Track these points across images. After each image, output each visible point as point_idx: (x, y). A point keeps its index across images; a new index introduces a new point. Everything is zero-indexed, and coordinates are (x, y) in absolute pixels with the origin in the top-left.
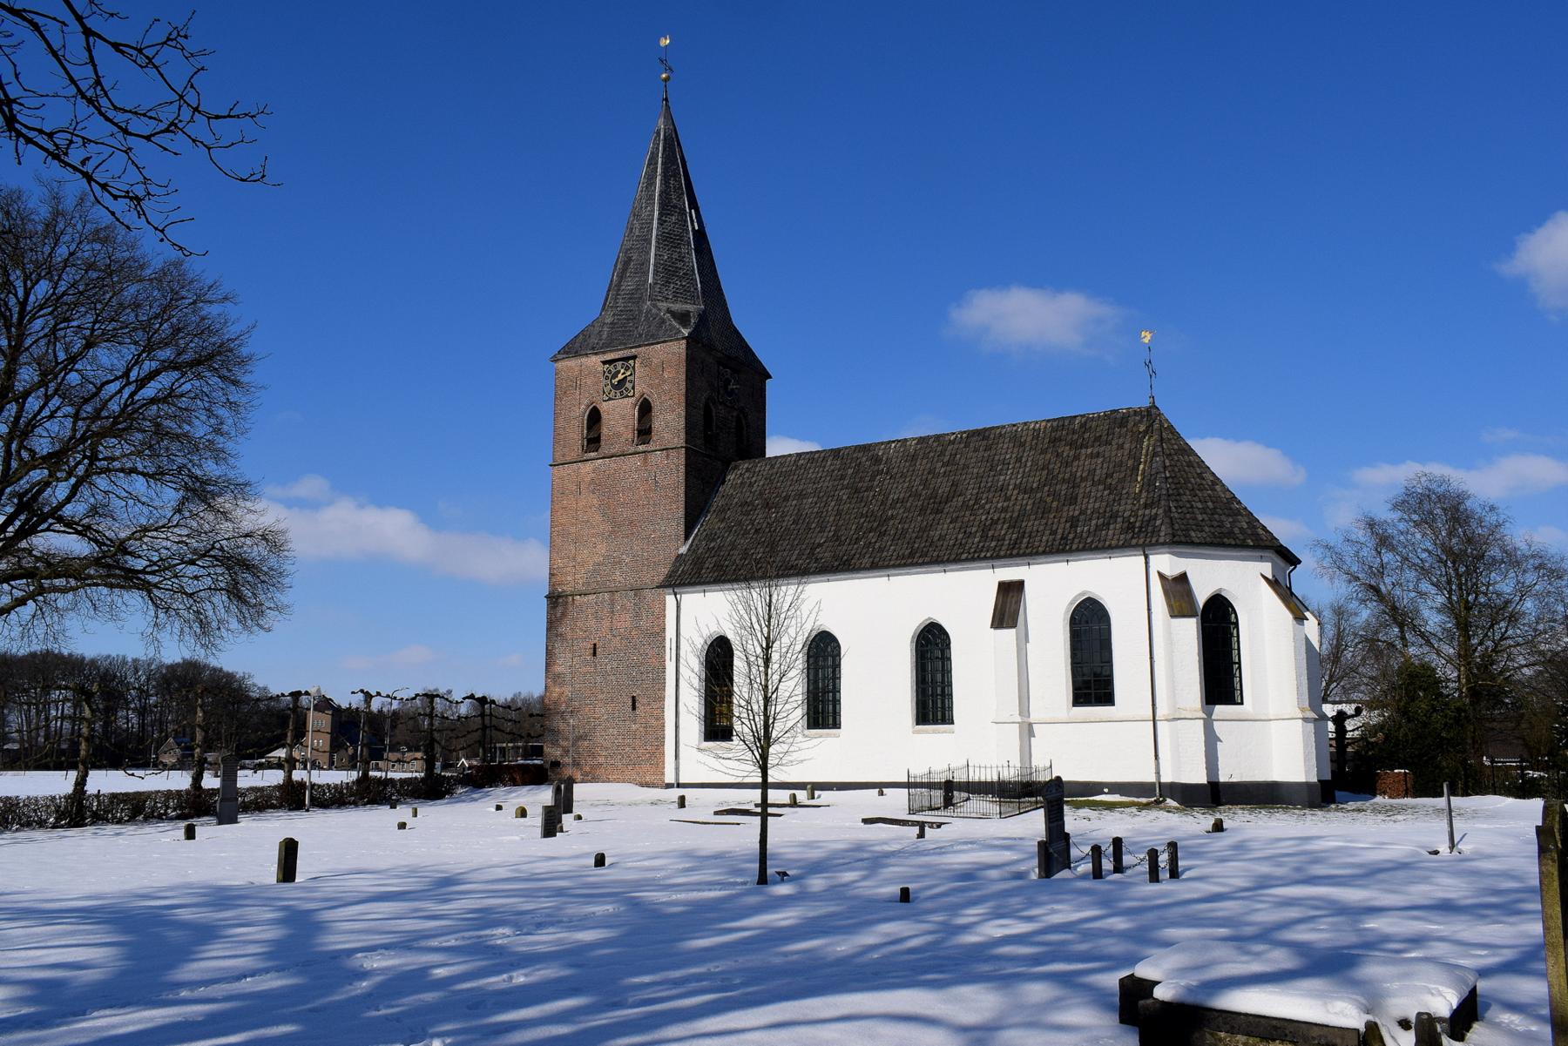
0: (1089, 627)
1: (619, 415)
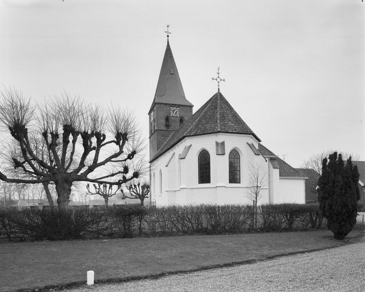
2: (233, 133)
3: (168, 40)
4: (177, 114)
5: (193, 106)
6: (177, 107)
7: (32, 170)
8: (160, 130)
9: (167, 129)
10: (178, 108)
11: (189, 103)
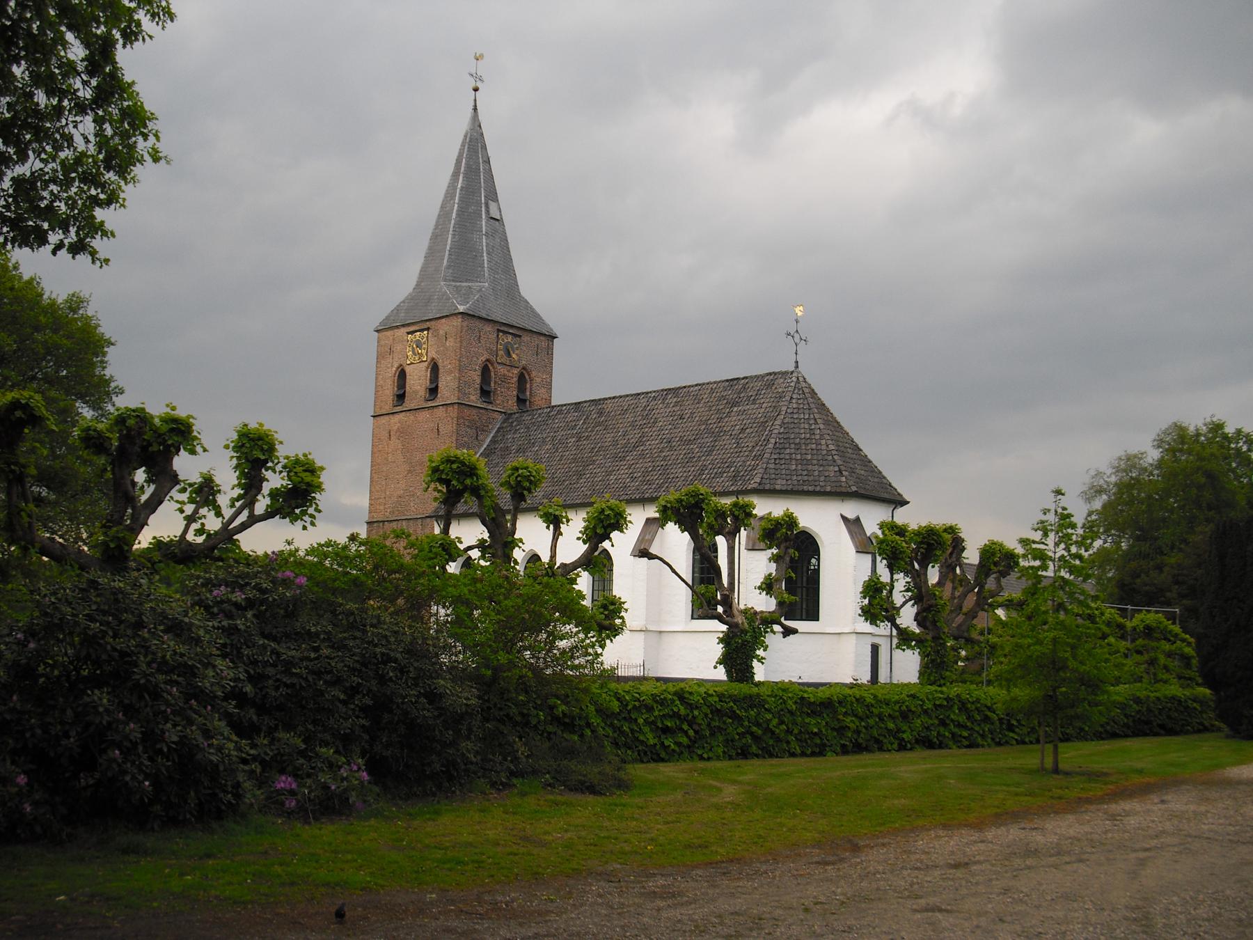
1: (418, 380)
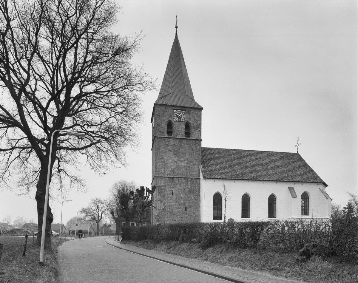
0: (305, 197)
2: (272, 181)
3: (176, 31)
4: (182, 118)
5: (202, 109)
6: (182, 110)
7: (30, 149)
8: (193, 139)
9: (187, 138)
10: (184, 111)
11: (199, 105)
